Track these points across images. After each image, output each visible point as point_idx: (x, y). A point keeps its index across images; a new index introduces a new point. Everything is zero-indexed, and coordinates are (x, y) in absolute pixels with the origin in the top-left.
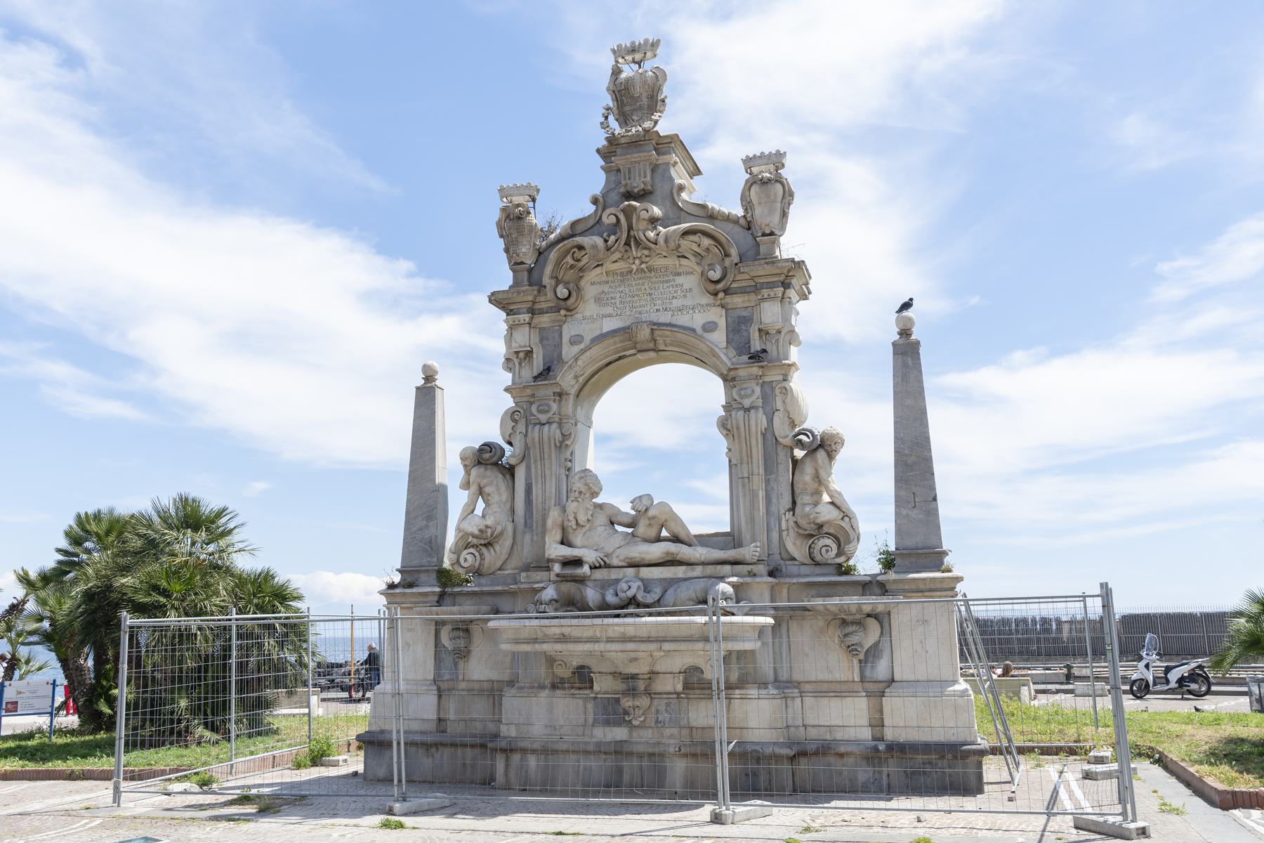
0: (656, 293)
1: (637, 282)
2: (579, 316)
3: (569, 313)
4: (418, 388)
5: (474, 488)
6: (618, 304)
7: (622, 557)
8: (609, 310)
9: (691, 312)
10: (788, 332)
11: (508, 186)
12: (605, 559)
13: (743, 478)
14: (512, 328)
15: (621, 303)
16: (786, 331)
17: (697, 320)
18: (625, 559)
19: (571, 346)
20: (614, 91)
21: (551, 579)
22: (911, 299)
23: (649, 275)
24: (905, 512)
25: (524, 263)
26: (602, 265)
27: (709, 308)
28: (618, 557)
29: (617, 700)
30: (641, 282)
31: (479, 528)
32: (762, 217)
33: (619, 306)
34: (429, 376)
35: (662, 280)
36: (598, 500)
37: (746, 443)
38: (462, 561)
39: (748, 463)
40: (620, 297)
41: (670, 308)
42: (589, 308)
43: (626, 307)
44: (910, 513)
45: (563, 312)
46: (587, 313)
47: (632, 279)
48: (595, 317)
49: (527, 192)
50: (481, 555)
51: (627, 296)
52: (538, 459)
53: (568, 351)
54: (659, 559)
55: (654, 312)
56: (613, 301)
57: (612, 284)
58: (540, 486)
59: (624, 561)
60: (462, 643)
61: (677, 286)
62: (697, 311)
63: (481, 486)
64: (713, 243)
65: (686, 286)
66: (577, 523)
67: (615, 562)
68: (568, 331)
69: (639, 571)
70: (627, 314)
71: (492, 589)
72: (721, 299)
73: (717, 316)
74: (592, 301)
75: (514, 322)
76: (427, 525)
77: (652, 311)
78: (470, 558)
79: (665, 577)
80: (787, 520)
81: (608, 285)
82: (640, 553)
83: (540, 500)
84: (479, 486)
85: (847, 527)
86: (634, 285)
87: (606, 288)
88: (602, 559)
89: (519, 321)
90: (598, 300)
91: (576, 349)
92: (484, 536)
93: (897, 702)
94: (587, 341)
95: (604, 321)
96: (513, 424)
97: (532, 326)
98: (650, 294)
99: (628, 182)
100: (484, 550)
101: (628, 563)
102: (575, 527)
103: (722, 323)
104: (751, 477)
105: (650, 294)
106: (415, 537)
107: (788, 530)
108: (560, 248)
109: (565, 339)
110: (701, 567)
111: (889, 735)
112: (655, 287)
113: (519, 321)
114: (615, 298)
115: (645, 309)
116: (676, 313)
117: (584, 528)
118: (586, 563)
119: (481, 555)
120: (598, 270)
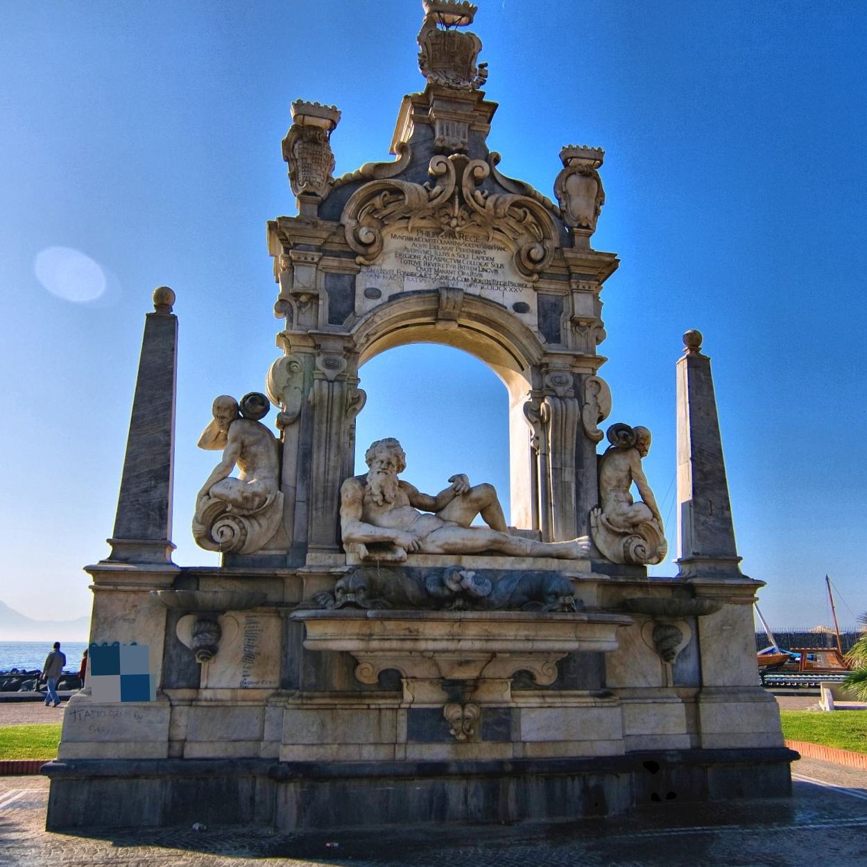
1: (444, 246)
3: (367, 263)
4: (148, 316)
5: (233, 447)
6: (422, 264)
7: (439, 543)
8: (411, 269)
9: (502, 288)
10: (596, 327)
11: (308, 103)
12: (420, 543)
14: (291, 265)
16: (595, 326)
18: (444, 545)
19: (366, 299)
20: (425, 43)
21: (348, 563)
24: (702, 518)
26: (409, 218)
27: (521, 289)
28: (433, 542)
29: (441, 710)
30: (448, 246)
31: (245, 494)
32: (580, 205)
33: (422, 266)
35: (472, 249)
36: (401, 476)
37: (561, 432)
38: (214, 533)
39: (561, 453)
40: (425, 257)
41: (480, 281)
44: (708, 520)
45: (360, 259)
46: (386, 266)
47: (439, 242)
48: (395, 272)
49: (331, 116)
50: (243, 528)
52: (324, 419)
53: (363, 304)
54: (483, 547)
55: (462, 281)
56: (417, 260)
58: (322, 453)
59: (441, 547)
61: (487, 259)
62: (508, 289)
63: (246, 442)
64: (534, 221)
65: (497, 261)
66: (384, 500)
67: (430, 547)
68: (364, 282)
69: (460, 560)
70: (433, 276)
71: (252, 572)
72: (534, 282)
74: (393, 255)
77: (460, 279)
79: (491, 568)
80: (596, 517)
83: (322, 469)
86: (441, 248)
88: (417, 543)
89: (306, 258)
91: (371, 303)
92: (249, 506)
94: (385, 297)
95: (405, 279)
96: (289, 376)
98: (459, 262)
100: (246, 523)
101: (445, 550)
102: (381, 503)
103: (533, 305)
104: (563, 468)
105: (459, 262)
107: (597, 527)
108: (369, 186)
109: (360, 290)
110: (531, 559)
114: (418, 257)
115: (453, 275)
117: (389, 506)
118: (400, 546)
119: (243, 528)
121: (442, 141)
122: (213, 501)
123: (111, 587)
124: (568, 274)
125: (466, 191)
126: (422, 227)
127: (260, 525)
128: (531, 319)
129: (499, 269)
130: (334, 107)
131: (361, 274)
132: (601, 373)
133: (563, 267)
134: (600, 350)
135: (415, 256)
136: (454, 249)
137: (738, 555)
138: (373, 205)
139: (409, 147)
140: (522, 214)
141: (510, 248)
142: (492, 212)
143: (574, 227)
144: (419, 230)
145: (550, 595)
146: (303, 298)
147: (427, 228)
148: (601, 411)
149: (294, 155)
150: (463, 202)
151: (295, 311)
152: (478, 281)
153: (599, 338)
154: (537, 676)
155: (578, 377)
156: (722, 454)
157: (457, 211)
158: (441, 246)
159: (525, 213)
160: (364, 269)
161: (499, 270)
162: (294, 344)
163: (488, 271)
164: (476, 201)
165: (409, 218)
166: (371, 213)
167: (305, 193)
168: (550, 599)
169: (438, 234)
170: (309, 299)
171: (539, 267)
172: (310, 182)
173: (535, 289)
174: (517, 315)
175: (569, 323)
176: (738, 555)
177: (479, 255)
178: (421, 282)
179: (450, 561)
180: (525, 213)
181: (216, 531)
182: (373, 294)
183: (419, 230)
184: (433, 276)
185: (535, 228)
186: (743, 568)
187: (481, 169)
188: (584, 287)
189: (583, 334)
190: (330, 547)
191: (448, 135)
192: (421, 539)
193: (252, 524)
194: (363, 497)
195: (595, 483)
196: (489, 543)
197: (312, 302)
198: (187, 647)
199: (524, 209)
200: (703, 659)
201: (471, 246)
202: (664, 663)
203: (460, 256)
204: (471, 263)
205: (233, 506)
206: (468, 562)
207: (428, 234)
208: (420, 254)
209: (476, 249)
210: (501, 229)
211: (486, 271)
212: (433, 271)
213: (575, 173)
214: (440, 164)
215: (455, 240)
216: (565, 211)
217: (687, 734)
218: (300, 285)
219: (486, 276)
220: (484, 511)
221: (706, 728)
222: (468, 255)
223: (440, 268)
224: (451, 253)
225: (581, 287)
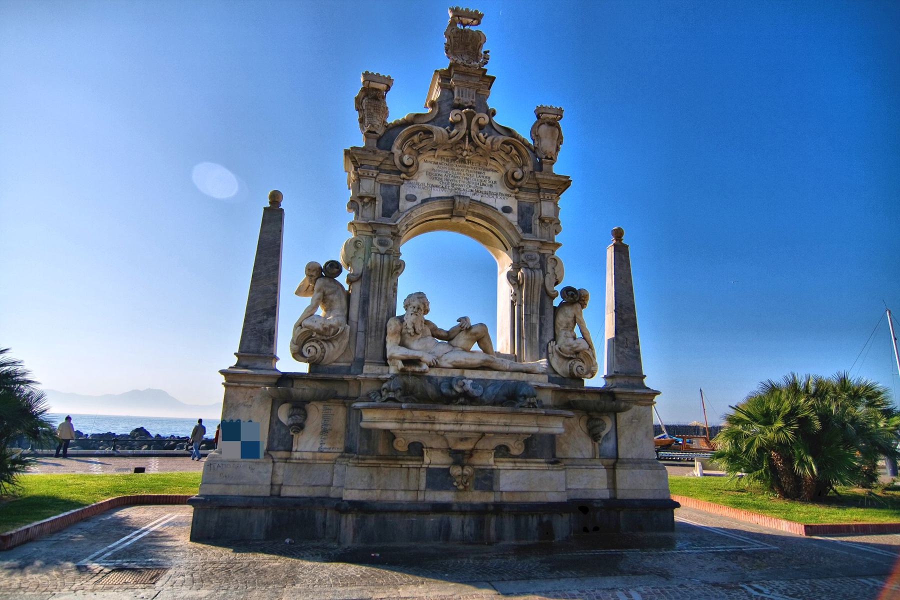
3: (408, 178)
4: (265, 209)
6: (444, 179)
7: (450, 361)
8: (436, 183)
9: (495, 197)
12: (438, 360)
15: (446, 179)
17: (499, 203)
18: (453, 362)
19: (406, 201)
24: (621, 350)
25: (376, 133)
29: (449, 469)
30: (461, 168)
31: (325, 326)
32: (547, 144)
33: (444, 181)
34: (275, 198)
36: (426, 317)
38: (304, 350)
42: (422, 179)
44: (624, 350)
45: (403, 175)
50: (323, 348)
52: (377, 279)
53: (404, 205)
56: (440, 177)
57: (440, 166)
58: (376, 300)
59: (451, 363)
60: (299, 419)
62: (499, 197)
64: (517, 154)
65: (493, 179)
66: (415, 332)
68: (405, 191)
69: (463, 372)
73: (512, 203)
74: (425, 173)
77: (468, 190)
78: (313, 350)
79: (483, 378)
81: (437, 165)
82: (465, 359)
83: (375, 311)
84: (324, 293)
85: (591, 354)
91: (410, 204)
92: (327, 334)
93: (621, 471)
94: (419, 201)
96: (355, 250)
97: (377, 180)
100: (325, 344)
101: (454, 365)
102: (413, 334)
103: (515, 208)
107: (553, 353)
108: (410, 129)
109: (403, 196)
110: (509, 373)
111: (620, 495)
114: (442, 175)
118: (425, 362)
119: (323, 348)
120: (432, 153)
121: (459, 100)
122: (304, 330)
125: (473, 133)
127: (334, 346)
128: (513, 217)
132: (558, 253)
134: (557, 239)
136: (465, 171)
138: (413, 140)
140: (509, 149)
142: (490, 147)
144: (442, 157)
145: (521, 396)
146: (366, 200)
150: (471, 140)
151: (360, 208)
153: (557, 231)
157: (467, 146)
158: (456, 168)
159: (511, 148)
160: (406, 182)
161: (493, 185)
167: (369, 132)
170: (370, 201)
171: (519, 183)
175: (538, 221)
179: (456, 373)
180: (511, 148)
183: (442, 157)
184: (450, 188)
186: (647, 382)
190: (379, 362)
192: (438, 358)
193: (328, 346)
194: (402, 330)
196: (482, 362)
206: (468, 374)
207: (448, 160)
209: (479, 171)
213: (544, 123)
215: (465, 165)
217: (607, 489)
219: (485, 189)
220: (479, 341)
223: (455, 183)
225: (546, 197)
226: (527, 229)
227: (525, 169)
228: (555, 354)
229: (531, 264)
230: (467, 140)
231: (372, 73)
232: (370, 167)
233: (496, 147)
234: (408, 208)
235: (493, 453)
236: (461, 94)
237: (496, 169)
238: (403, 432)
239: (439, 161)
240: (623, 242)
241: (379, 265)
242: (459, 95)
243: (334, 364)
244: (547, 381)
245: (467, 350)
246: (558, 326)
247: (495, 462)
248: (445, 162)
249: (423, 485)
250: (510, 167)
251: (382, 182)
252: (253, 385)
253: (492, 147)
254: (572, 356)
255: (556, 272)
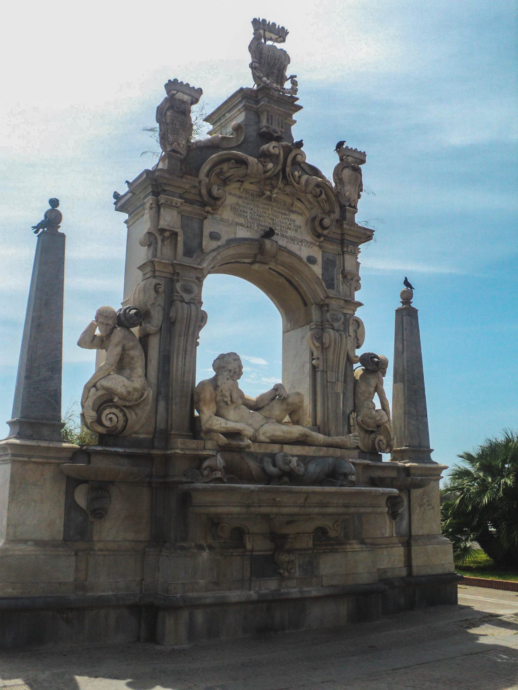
0: (277, 220)
2: (218, 217)
3: (212, 212)
6: (249, 217)
8: (242, 220)
9: (300, 244)
11: (352, 148)
13: (332, 382)
15: (251, 218)
17: (304, 252)
22: (406, 278)
23: (273, 204)
27: (312, 246)
28: (264, 434)
30: (266, 207)
33: (249, 220)
38: (103, 419)
39: (335, 372)
41: (286, 236)
43: (254, 222)
45: (208, 209)
47: (260, 202)
50: (125, 415)
51: (256, 214)
52: (183, 333)
53: (208, 244)
56: (245, 214)
57: (245, 201)
59: (268, 438)
61: (291, 220)
62: (303, 245)
63: (126, 347)
64: (326, 199)
65: (298, 223)
66: (231, 401)
68: (209, 227)
72: (321, 242)
73: (318, 255)
75: (166, 201)
76: (52, 377)
87: (240, 202)
89: (171, 203)
90: (234, 209)
91: (214, 244)
95: (237, 228)
98: (273, 220)
99: (270, 126)
102: (229, 403)
104: (336, 382)
105: (273, 220)
106: (38, 388)
107: (354, 426)
109: (206, 233)
110: (325, 448)
112: (276, 216)
113: (176, 204)
116: (290, 241)
119: (125, 415)
121: (268, 128)
122: (100, 393)
123: (26, 459)
124: (341, 239)
125: (288, 169)
126: (249, 190)
127: (136, 414)
128: (317, 269)
129: (298, 229)
130: (364, 152)
131: (207, 219)
132: (359, 313)
133: (339, 234)
134: (358, 296)
135: (244, 211)
136: (270, 210)
137: (431, 448)
138: (221, 169)
139: (243, 127)
140: (319, 193)
141: (305, 215)
142: (303, 189)
143: (347, 206)
144: (246, 191)
146: (167, 234)
147: (253, 191)
148: (358, 343)
149: (166, 120)
150: (285, 177)
151: (160, 243)
152: (285, 236)
153: (357, 288)
154: (329, 530)
155: (345, 314)
156: (423, 378)
157: (280, 183)
158: (261, 206)
159: (321, 192)
160: (210, 217)
161: (298, 230)
162: (158, 269)
163: (291, 229)
164: (294, 180)
165: (243, 182)
166: (218, 174)
167: (173, 151)
168: (341, 478)
169: (260, 196)
170: (171, 234)
171: (325, 232)
172: (178, 143)
173: (320, 247)
174: (309, 264)
175: (341, 276)
176: (431, 448)
177: (285, 217)
178: (248, 231)
179: (275, 448)
180: (321, 192)
181: (105, 415)
182: (214, 236)
183: (246, 191)
184: (256, 228)
185: (325, 203)
186: (434, 456)
187: (301, 156)
188: (351, 250)
189: (348, 284)
190: (185, 434)
191: (272, 124)
193: (130, 413)
194: (216, 397)
195: (352, 394)
197: (172, 237)
198: (81, 508)
199: (321, 189)
200: (412, 517)
201: (281, 208)
202: (391, 520)
203: (273, 216)
204: (280, 221)
205: (119, 398)
206: (287, 448)
207: (252, 195)
208: (247, 210)
209: (284, 211)
210: (302, 200)
211: (290, 229)
212: (256, 224)
213: (348, 167)
214: (275, 148)
215: (270, 202)
216: (340, 192)
217: (404, 567)
218: (166, 223)
219: (290, 233)
221: (414, 563)
222: (279, 216)
223: (261, 223)
224: (268, 212)
225: (349, 250)
226: (331, 285)
227: (332, 216)
228: (357, 427)
229: (336, 325)
230: (281, 178)
231: (182, 82)
232: (173, 194)
233: (310, 188)
234: (212, 248)
235: (312, 537)
236: (270, 121)
237: (300, 212)
238: (230, 516)
239: (244, 195)
240: (412, 305)
241: (185, 316)
242: (268, 122)
243: (134, 435)
244: (357, 457)
245: (279, 422)
246: (360, 396)
247: (314, 545)
248: (250, 197)
249: (248, 574)
250: (316, 211)
251: (183, 213)
252: (45, 460)
253: (306, 189)
254: (374, 429)
255: (358, 335)
